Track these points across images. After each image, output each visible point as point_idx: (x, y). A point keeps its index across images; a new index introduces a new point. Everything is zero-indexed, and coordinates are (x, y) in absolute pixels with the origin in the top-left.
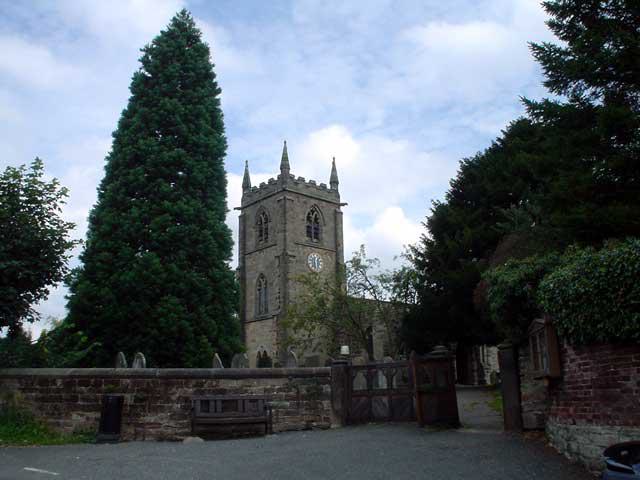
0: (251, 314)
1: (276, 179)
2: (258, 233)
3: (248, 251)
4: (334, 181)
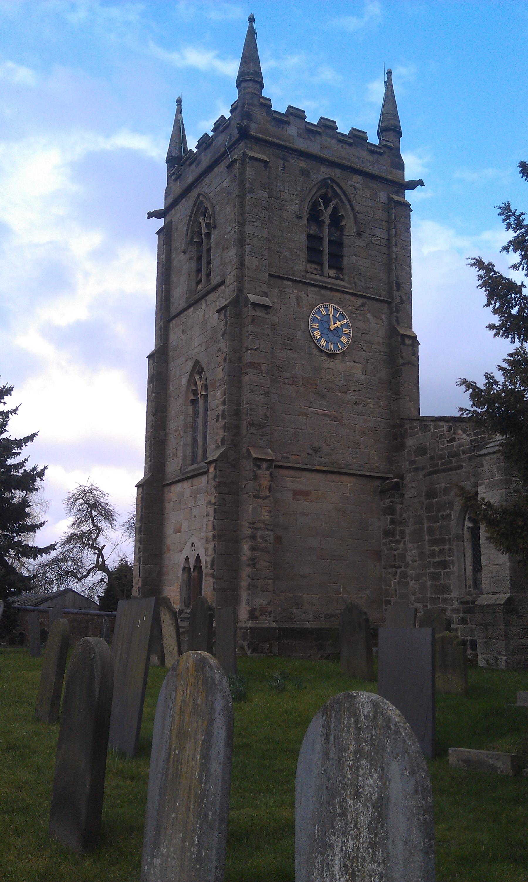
1: (228, 115)
2: (193, 266)
3: (174, 311)
4: (390, 127)
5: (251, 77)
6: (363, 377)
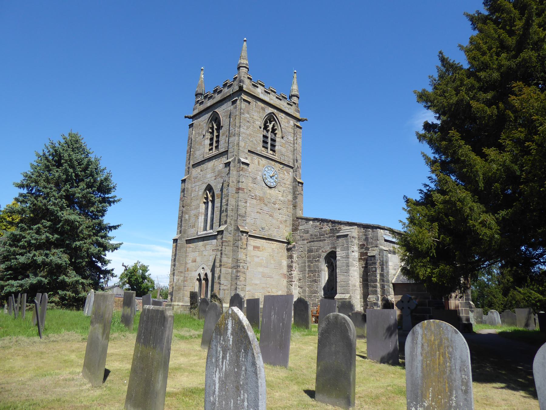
5: (244, 65)
6: (282, 198)
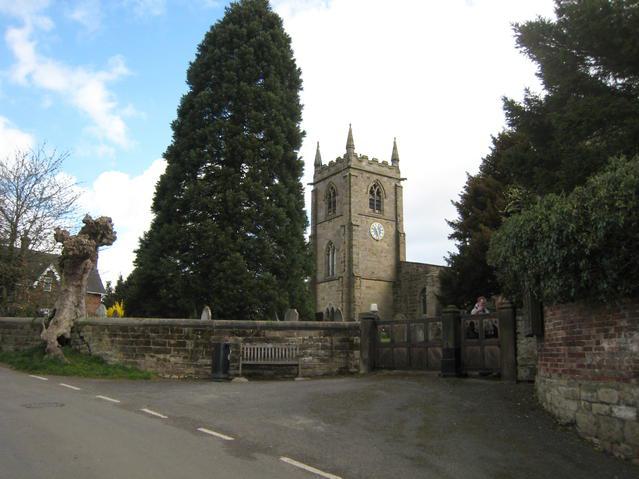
0: (320, 276)
2: (327, 206)
4: (395, 159)
